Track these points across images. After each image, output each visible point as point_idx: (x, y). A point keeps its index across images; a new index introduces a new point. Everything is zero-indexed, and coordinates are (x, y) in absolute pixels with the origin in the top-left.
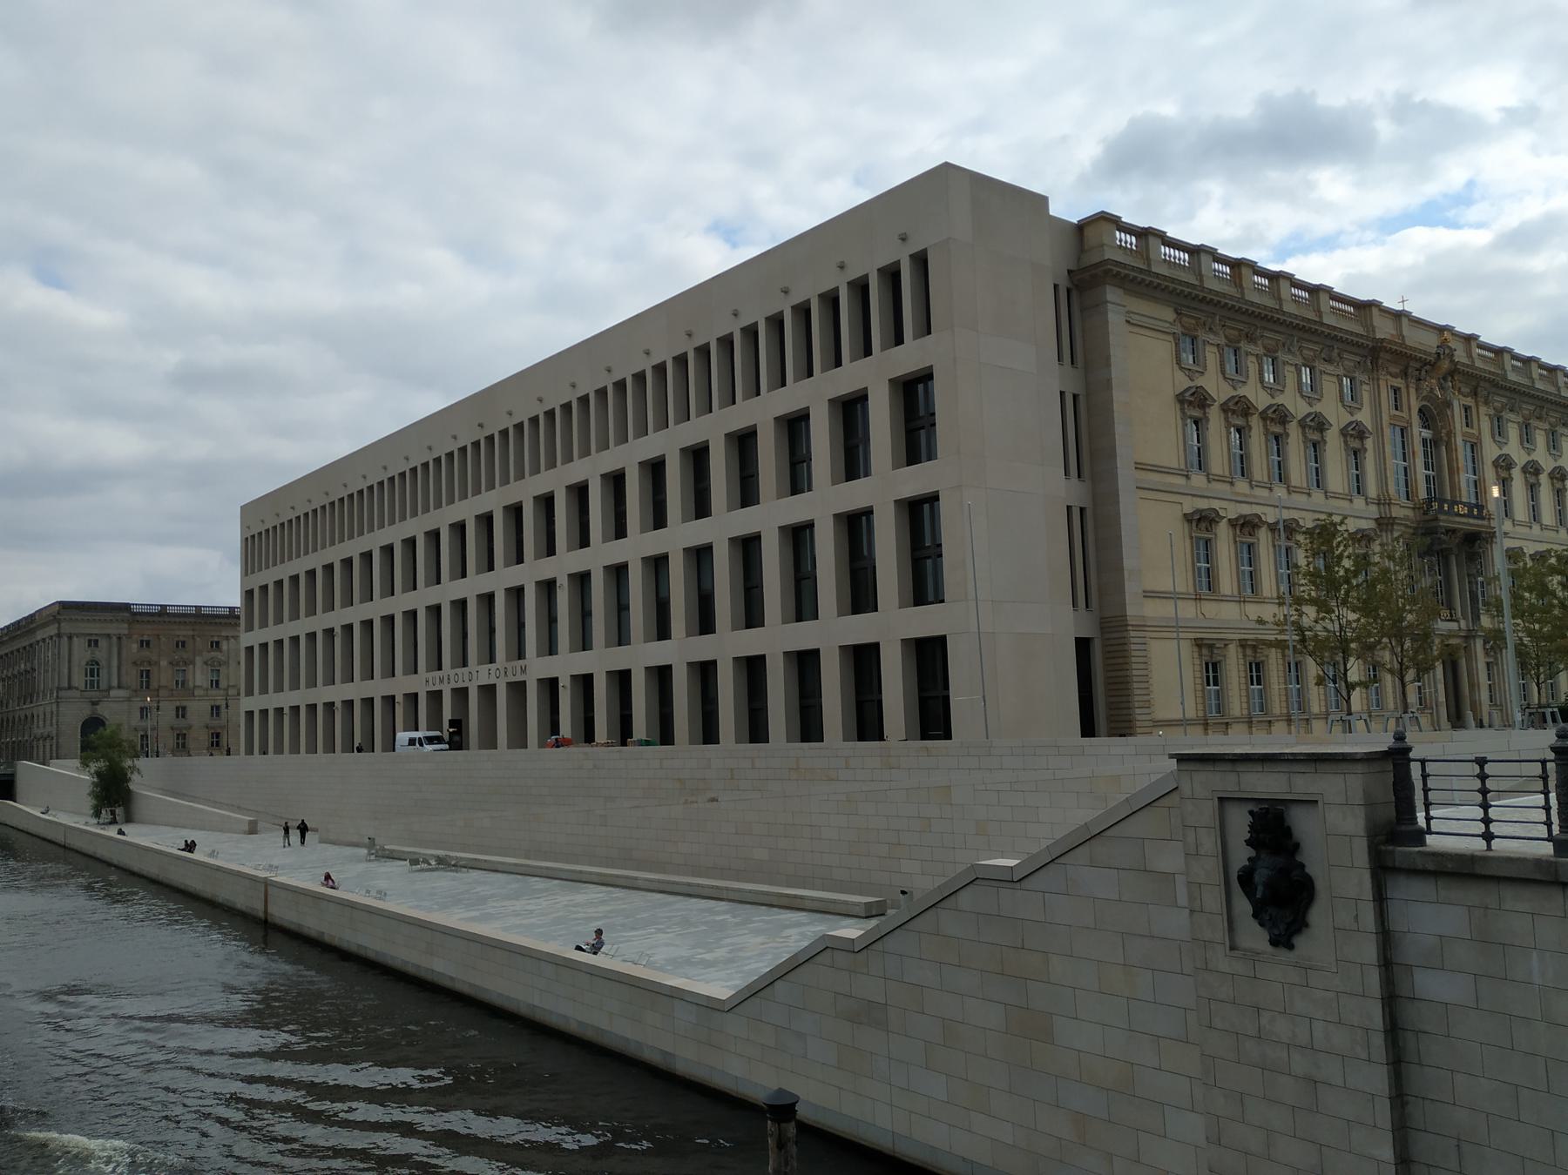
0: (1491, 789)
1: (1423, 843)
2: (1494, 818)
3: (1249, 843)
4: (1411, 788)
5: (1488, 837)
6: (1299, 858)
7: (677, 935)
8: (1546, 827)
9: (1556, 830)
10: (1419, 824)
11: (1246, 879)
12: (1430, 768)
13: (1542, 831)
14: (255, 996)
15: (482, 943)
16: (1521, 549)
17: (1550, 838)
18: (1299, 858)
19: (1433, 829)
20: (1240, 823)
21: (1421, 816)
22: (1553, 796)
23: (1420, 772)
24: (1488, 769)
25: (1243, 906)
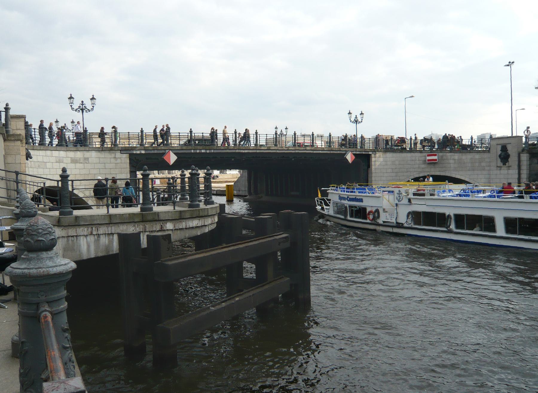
3: (501, 151)
6: (508, 152)
11: (500, 156)
18: (508, 152)
20: (499, 148)
25: (499, 160)
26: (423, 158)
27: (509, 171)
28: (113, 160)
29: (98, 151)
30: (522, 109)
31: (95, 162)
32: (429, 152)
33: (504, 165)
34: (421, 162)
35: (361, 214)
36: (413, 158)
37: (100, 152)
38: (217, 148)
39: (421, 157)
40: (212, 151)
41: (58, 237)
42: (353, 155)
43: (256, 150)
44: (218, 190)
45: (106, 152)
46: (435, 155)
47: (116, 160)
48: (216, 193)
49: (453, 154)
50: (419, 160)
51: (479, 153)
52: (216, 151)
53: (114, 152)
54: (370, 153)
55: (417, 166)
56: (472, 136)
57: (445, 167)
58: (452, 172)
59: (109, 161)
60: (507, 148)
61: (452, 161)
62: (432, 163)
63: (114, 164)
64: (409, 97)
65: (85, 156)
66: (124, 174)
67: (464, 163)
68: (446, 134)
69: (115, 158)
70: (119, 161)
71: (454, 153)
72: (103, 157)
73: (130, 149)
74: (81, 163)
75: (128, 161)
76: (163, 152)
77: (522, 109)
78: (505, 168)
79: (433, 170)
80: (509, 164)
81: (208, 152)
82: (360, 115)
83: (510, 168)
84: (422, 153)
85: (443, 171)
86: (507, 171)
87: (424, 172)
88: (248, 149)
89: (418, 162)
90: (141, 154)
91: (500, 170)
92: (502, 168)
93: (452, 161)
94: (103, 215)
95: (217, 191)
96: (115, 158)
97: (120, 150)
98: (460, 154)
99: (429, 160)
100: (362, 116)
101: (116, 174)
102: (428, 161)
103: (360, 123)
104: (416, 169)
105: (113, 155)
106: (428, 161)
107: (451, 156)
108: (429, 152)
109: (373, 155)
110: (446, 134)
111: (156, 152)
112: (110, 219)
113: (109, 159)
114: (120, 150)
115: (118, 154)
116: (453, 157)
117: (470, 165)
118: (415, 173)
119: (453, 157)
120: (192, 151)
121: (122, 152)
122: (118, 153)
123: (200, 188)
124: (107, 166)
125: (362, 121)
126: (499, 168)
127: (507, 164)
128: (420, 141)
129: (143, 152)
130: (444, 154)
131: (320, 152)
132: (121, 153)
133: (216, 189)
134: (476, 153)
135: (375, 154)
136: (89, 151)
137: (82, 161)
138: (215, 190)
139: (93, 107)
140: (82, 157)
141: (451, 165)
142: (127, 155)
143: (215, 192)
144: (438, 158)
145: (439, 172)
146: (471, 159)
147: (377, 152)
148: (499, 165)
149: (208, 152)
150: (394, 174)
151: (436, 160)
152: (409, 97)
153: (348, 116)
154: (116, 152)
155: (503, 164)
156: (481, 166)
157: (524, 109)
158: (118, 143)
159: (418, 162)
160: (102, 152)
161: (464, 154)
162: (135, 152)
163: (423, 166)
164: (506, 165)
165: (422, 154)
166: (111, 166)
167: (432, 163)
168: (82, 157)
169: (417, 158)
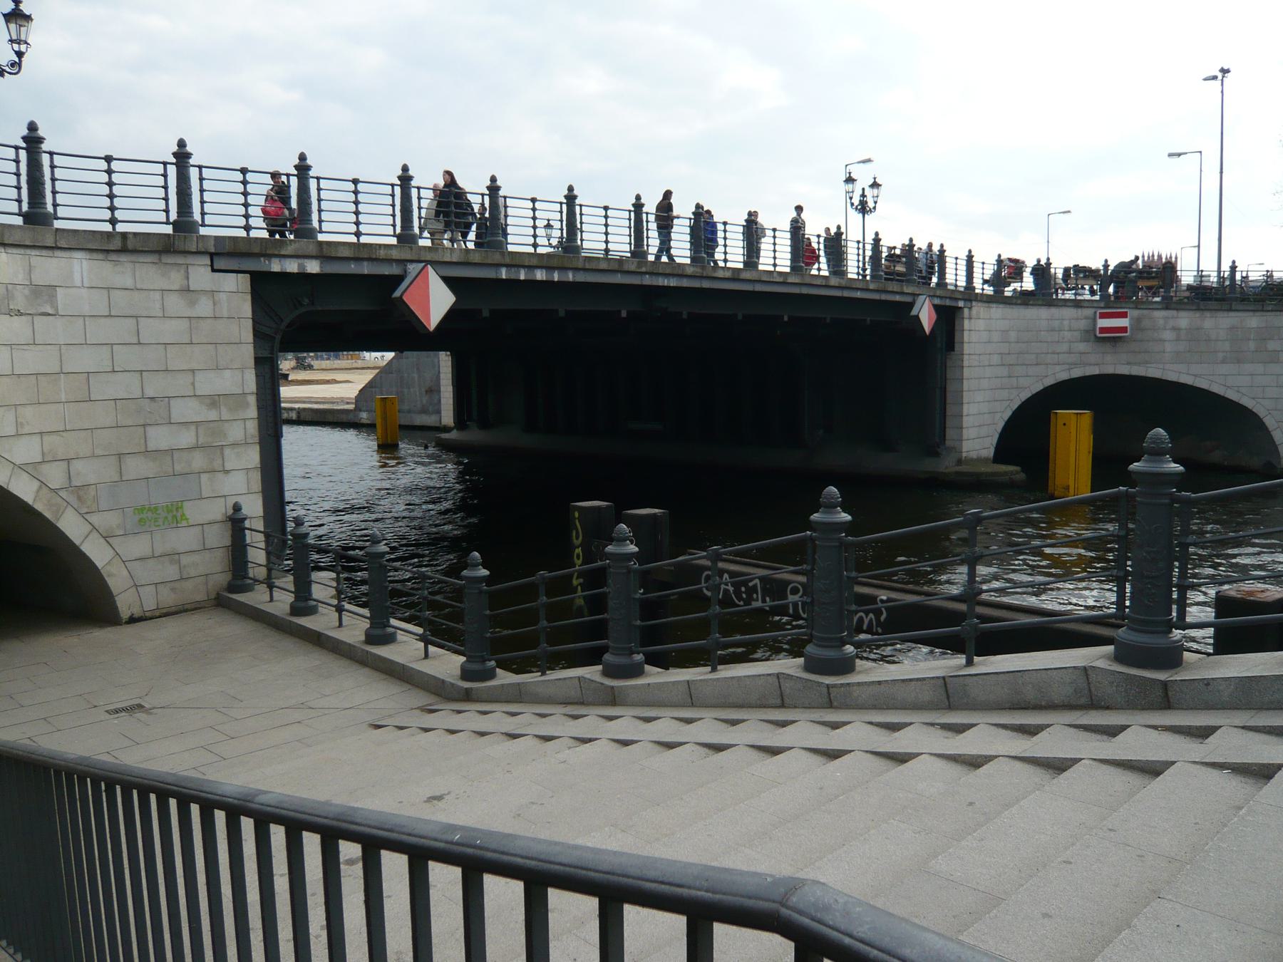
0: (250, 181)
1: (416, 243)
2: (362, 211)
4: (310, 204)
5: (775, 265)
7: (236, 522)
8: (165, 213)
9: (25, 207)
10: (195, 218)
12: (323, 184)
13: (390, 230)
14: (1233, 534)
15: (1026, 365)
16: (1092, 296)
17: (394, 235)
19: (59, 215)
21: (315, 217)
22: (645, 243)
23: (198, 176)
24: (249, 177)
26: (1083, 324)
28: (175, 304)
29: (101, 256)
30: (1179, 155)
31: (86, 310)
32: (1102, 305)
34: (1077, 334)
36: (1056, 323)
37: (113, 257)
38: (587, 266)
39: (1077, 319)
40: (570, 277)
42: (932, 306)
43: (702, 277)
44: (304, 409)
45: (142, 258)
46: (1124, 315)
47: (192, 303)
48: (298, 417)
49: (1174, 313)
50: (1071, 330)
52: (581, 277)
53: (180, 260)
54: (961, 304)
55: (1065, 347)
56: (1234, 262)
57: (1146, 352)
58: (1167, 366)
59: (158, 305)
61: (1168, 335)
62: (1112, 339)
63: (184, 324)
64: (859, 162)
65: (38, 279)
66: (227, 373)
68: (1039, 261)
69: (186, 290)
70: (204, 307)
71: (1177, 310)
72: (129, 283)
73: (256, 250)
74: (20, 314)
75: (247, 309)
76: (394, 270)
79: (1109, 358)
81: (556, 279)
82: (843, 184)
84: (1081, 307)
85: (1139, 364)
87: (1085, 364)
88: (680, 272)
89: (1067, 335)
90: (304, 277)
93: (1168, 335)
95: (299, 411)
96: (186, 290)
97: (212, 255)
98: (1198, 314)
99: (1103, 330)
100: (875, 191)
101: (193, 371)
102: (1100, 333)
103: (871, 212)
104: (1061, 356)
105: (176, 279)
106: (1100, 333)
107: (1166, 318)
108: (1102, 305)
109: (966, 311)
110: (1039, 261)
111: (366, 272)
113: (157, 295)
114: (212, 255)
115: (200, 274)
116: (1171, 323)
117: (1227, 346)
118: (1058, 368)
119: (1171, 323)
120: (504, 274)
121: (220, 263)
122: (202, 270)
123: (283, 405)
124: (150, 330)
125: (875, 208)
128: (1062, 271)
129: (313, 267)
130: (1145, 312)
131: (859, 295)
132: (214, 270)
133: (297, 406)
134: (1251, 314)
135: (970, 308)
136: (58, 253)
137: (19, 302)
138: (292, 409)
139: (20, 54)
140: (20, 278)
141: (1167, 344)
142: (243, 281)
143: (294, 416)
144: (1130, 324)
145: (1129, 367)
146: (1232, 328)
147: (974, 303)
149: (556, 277)
150: (1003, 371)
151: (1124, 329)
152: (859, 162)
153: (844, 187)
154: (190, 260)
157: (1069, 212)
158: (197, 216)
159: (1067, 335)
160: (123, 258)
161: (1208, 314)
162: (276, 266)
163: (1082, 347)
165: (1080, 310)
166: (173, 330)
167: (1114, 337)
168: (20, 278)
169: (1066, 323)
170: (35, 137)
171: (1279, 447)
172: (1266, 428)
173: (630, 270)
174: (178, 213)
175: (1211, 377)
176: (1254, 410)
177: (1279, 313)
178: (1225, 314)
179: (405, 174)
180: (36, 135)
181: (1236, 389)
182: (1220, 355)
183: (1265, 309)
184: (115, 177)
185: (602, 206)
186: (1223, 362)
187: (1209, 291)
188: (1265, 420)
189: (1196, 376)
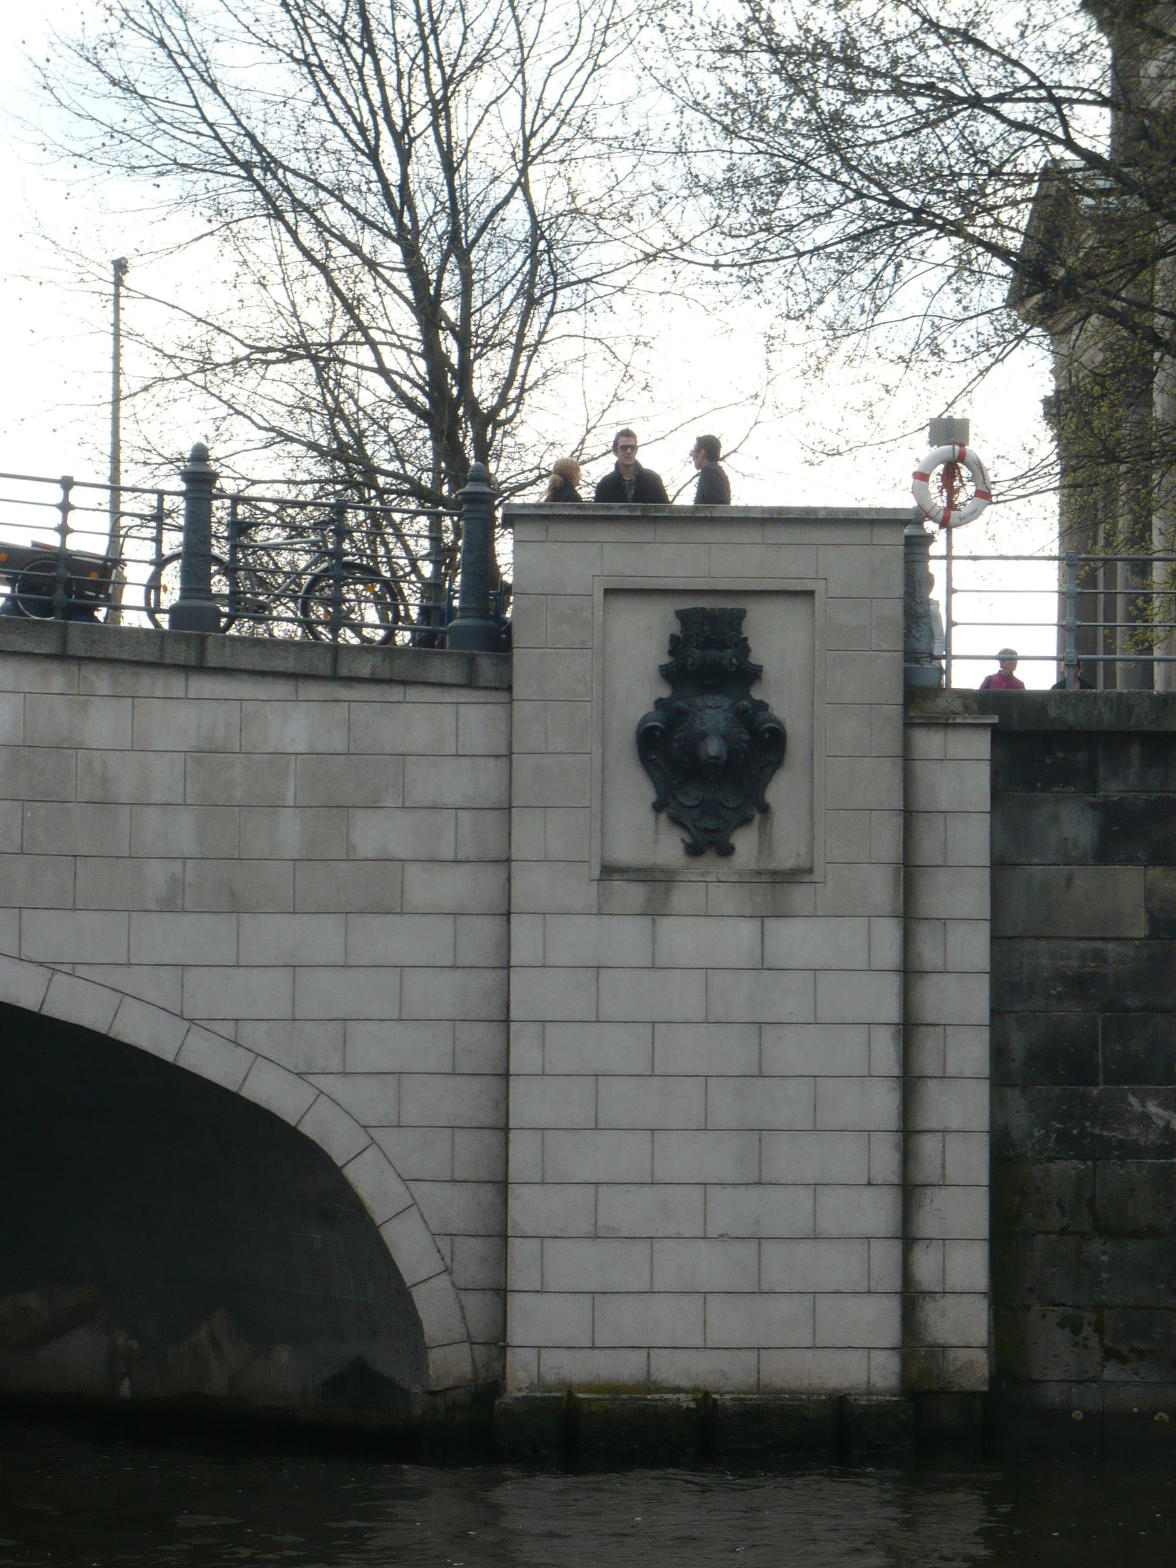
18: (757, 694)
27: (667, 925)
33: (709, 861)
35: (364, 1524)
41: (722, 84)
51: (314, 691)
60: (743, 647)
67: (105, 803)
77: (197, 239)
78: (725, 897)
80: (766, 845)
83: (800, 895)
86: (746, 930)
91: (655, 911)
92: (683, 897)
94: (504, 1366)
98: (57, 679)
112: (335, 660)
126: (633, 893)
127: (745, 842)
134: (282, 689)
148: (625, 852)
155: (694, 850)
156: (350, 858)
164: (726, 851)
170: (204, 473)
171: (415, 1292)
172: (358, 1209)
173: (360, 675)
174: (668, 674)
175: (53, 966)
176: (306, 1129)
177: (396, 693)
178: (177, 684)
179: (199, 468)
180: (206, 470)
181: (227, 1030)
182: (158, 874)
183: (343, 672)
184: (56, 517)
185: (59, 478)
186: (171, 905)
187: (94, 577)
188: (350, 1173)
189: (51, 967)
